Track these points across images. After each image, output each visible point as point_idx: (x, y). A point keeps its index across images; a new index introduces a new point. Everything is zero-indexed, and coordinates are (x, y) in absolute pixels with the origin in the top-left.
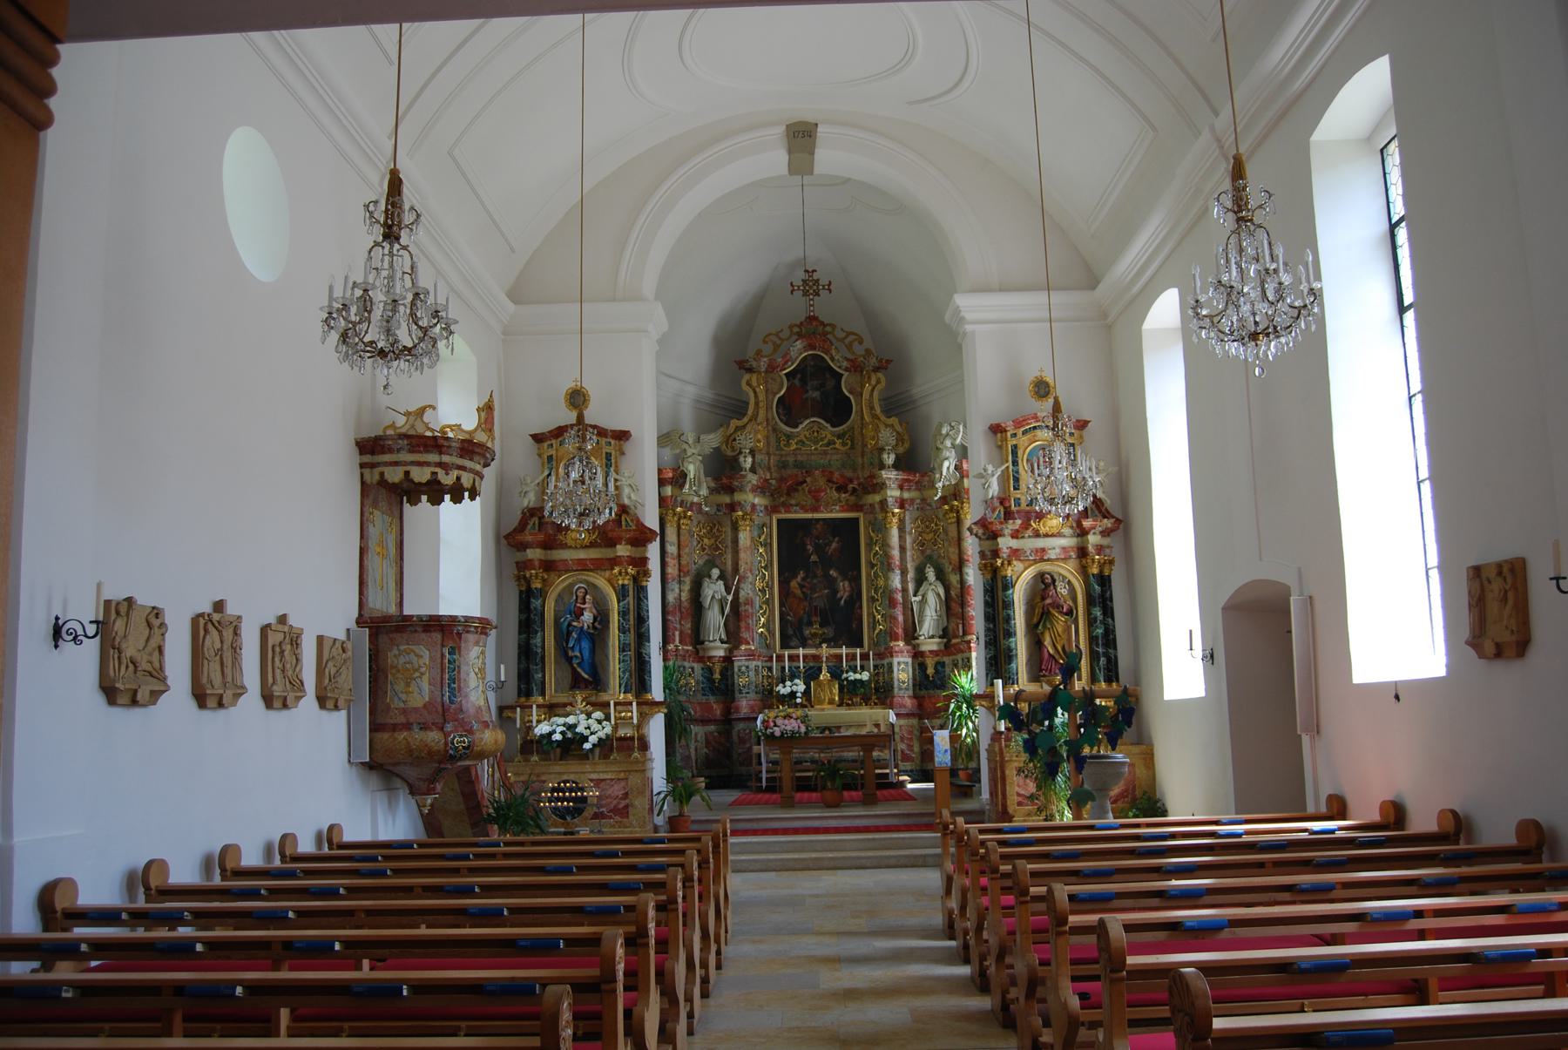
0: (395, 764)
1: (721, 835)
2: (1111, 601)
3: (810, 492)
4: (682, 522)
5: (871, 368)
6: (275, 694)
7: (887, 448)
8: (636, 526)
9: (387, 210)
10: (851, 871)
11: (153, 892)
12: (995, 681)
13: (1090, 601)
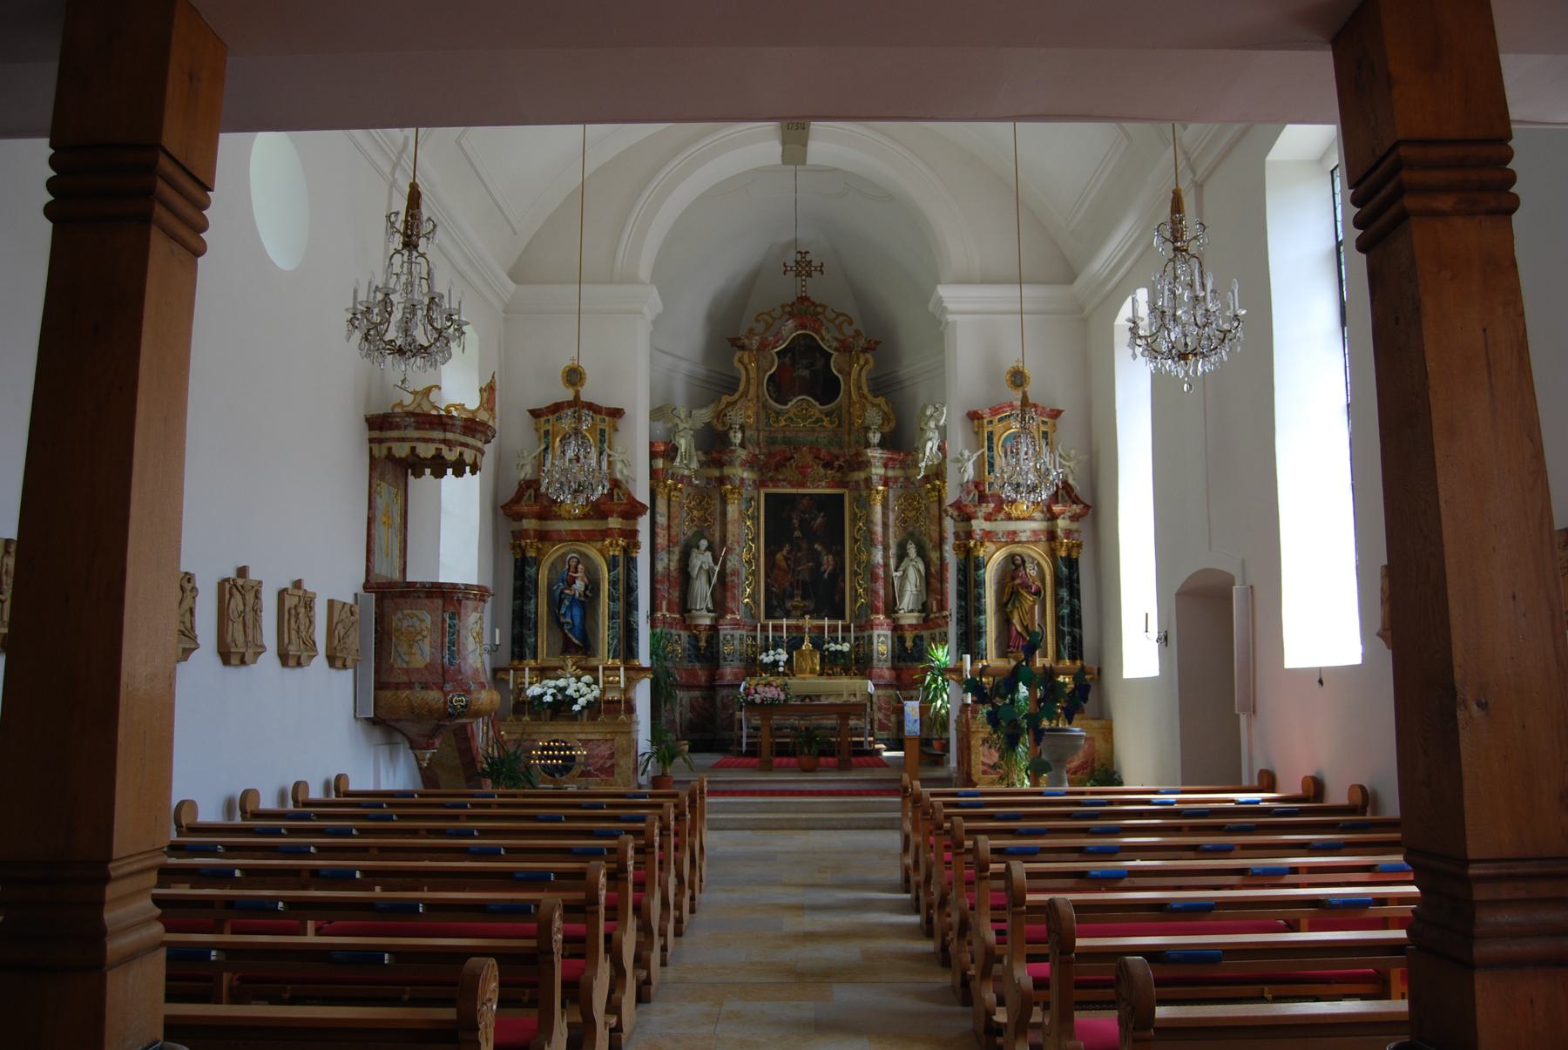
0: (398, 720)
1: (698, 792)
2: (1078, 582)
3: (797, 467)
4: (672, 494)
5: (860, 349)
6: (291, 653)
7: (873, 427)
8: (627, 499)
9: (406, 222)
10: (823, 832)
11: (184, 829)
12: (964, 656)
13: (1058, 582)
